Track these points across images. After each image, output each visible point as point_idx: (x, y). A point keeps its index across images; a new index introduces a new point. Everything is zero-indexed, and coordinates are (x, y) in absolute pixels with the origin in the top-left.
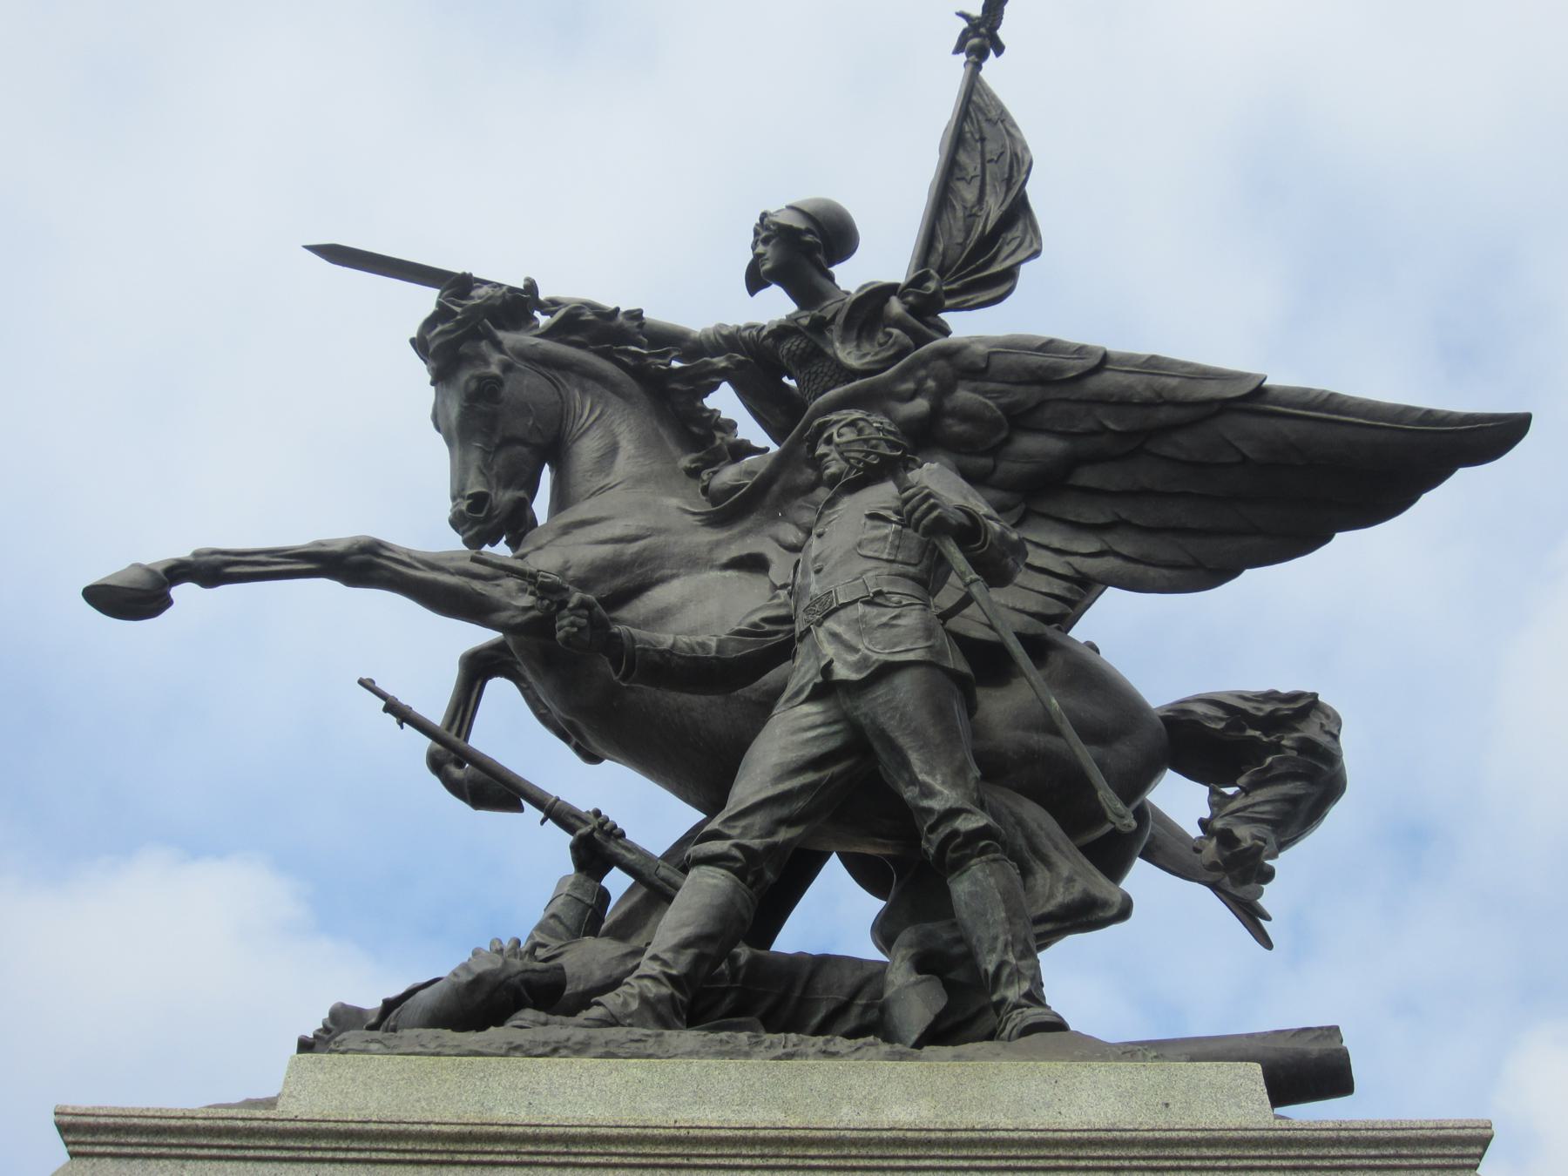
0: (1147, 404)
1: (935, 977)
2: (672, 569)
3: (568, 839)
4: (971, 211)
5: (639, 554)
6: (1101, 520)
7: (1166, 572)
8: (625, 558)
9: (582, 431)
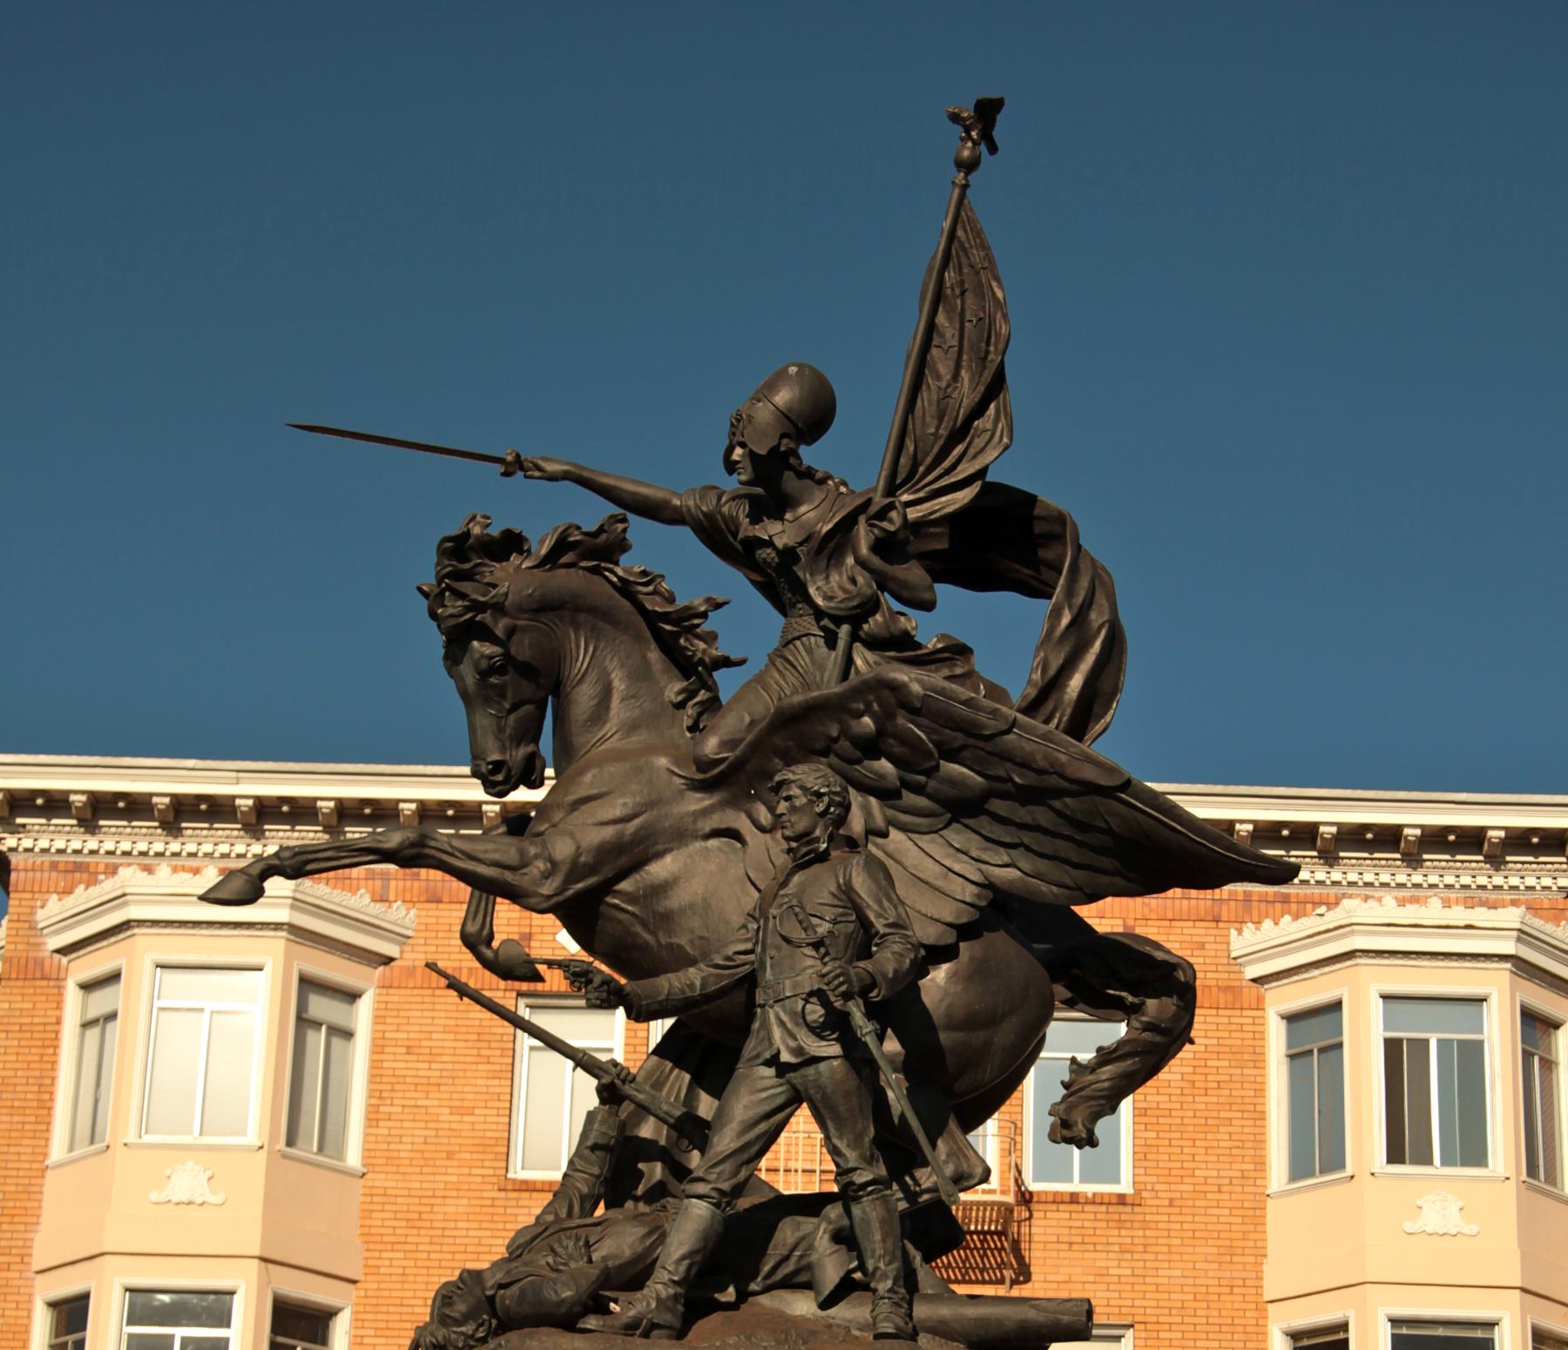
0: (1041, 772)
1: (843, 1247)
2: (664, 844)
3: (594, 1082)
4: (945, 392)
5: (636, 833)
6: (1007, 840)
7: (1055, 889)
8: (626, 839)
9: (579, 676)
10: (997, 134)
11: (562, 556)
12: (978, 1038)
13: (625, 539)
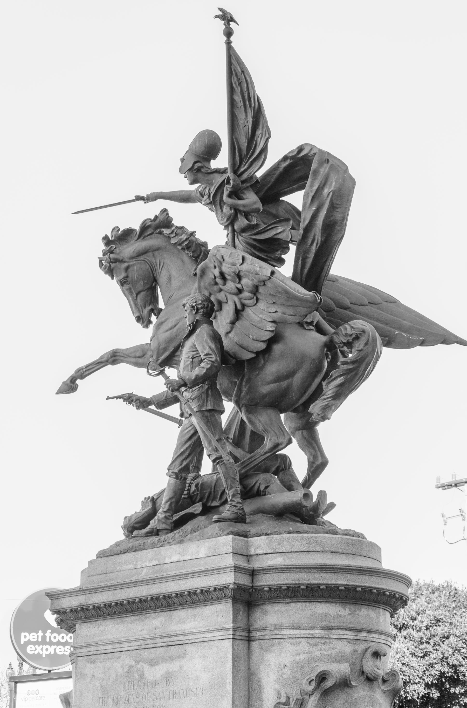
10: (218, 19)
11: (281, 197)
12: (284, 384)
13: (169, 217)
